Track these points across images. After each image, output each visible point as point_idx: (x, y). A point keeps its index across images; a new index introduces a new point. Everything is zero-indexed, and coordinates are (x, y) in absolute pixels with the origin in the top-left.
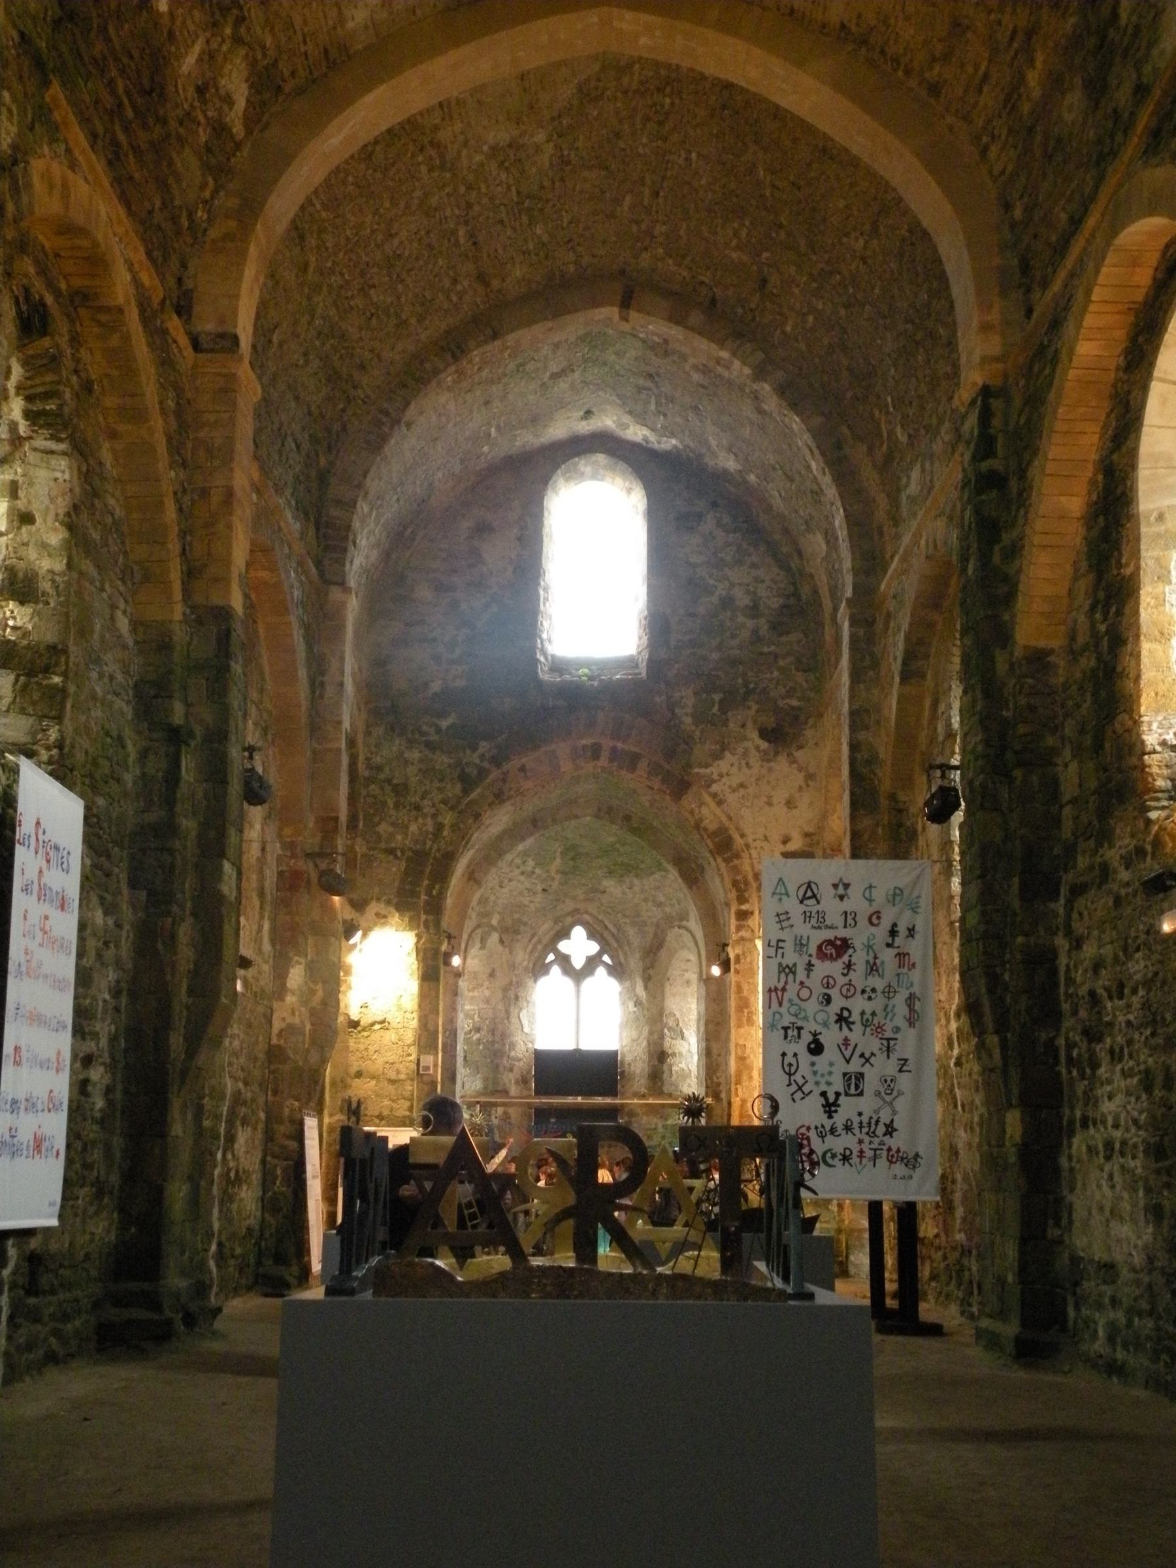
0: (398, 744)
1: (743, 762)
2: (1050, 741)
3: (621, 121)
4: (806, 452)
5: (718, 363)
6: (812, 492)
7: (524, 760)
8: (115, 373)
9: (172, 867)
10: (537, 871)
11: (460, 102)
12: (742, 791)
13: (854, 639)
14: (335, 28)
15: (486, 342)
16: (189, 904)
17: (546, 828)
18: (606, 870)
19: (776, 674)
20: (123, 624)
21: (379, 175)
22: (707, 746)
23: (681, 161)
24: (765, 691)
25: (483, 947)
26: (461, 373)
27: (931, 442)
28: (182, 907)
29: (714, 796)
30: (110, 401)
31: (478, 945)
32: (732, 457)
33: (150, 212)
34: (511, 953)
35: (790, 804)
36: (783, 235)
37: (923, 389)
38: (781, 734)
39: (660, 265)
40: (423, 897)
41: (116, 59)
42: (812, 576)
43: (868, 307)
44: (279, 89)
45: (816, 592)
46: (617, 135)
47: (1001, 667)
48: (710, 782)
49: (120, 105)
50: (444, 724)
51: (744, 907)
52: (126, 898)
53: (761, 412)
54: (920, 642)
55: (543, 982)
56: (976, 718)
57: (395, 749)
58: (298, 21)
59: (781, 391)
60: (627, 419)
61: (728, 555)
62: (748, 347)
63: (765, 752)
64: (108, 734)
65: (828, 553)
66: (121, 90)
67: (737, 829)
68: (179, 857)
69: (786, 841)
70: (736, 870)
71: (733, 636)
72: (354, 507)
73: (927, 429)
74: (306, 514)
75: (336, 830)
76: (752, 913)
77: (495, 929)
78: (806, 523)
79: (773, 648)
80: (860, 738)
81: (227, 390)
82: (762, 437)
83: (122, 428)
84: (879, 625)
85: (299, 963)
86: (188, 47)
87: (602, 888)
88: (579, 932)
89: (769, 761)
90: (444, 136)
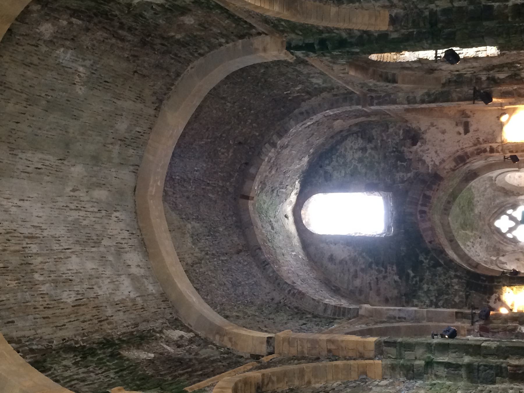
0: (420, 293)
1: (427, 152)
2: (427, 13)
3: (184, 196)
4: (303, 126)
5: (269, 162)
6: (318, 126)
7: (427, 242)
8: (286, 380)
9: (485, 366)
10: (472, 240)
11: (178, 253)
12: (438, 152)
13: (379, 104)
14: (155, 297)
15: (262, 252)
16: (502, 360)
17: (453, 236)
18: (471, 212)
19: (389, 140)
20: (384, 382)
21: (204, 287)
22: (420, 167)
23: (198, 173)
24: (397, 144)
25: (506, 263)
26: (273, 263)
27: (303, 74)
28: (502, 363)
29: (440, 163)
30: (297, 383)
31: (505, 265)
32: (303, 159)
33: (224, 366)
34: (508, 252)
35: (444, 132)
36: (224, 135)
37: (283, 78)
38: (414, 137)
39: (233, 184)
40: (487, 283)
41: (172, 372)
42: (350, 126)
43: (251, 102)
44: (176, 319)
45: (356, 125)
46: (188, 198)
47: (395, 35)
48: (435, 165)
49: (187, 372)
50: (412, 274)
51: (488, 149)
52: (500, 385)
53: (287, 146)
54: (381, 76)
55: (519, 239)
56: (417, 44)
57: (423, 295)
58: (153, 310)
59: (280, 136)
60: (288, 201)
61: (341, 161)
62: (264, 150)
63: (422, 143)
64: (431, 389)
65: (342, 119)
66: (181, 372)
67: (454, 154)
68: (481, 363)
69: (459, 134)
70: (472, 154)
71: (374, 157)
72: (327, 304)
73: (297, 76)
74: (331, 322)
75: (462, 313)
76: (491, 146)
77: (498, 258)
78: (329, 128)
79: (379, 141)
80: (419, 100)
81: (290, 342)
82: (294, 152)
83: (306, 379)
84: (373, 95)
85: (520, 329)
86: (164, 349)
87: (479, 214)
88: (498, 224)
89: (426, 142)
90: (190, 261)
